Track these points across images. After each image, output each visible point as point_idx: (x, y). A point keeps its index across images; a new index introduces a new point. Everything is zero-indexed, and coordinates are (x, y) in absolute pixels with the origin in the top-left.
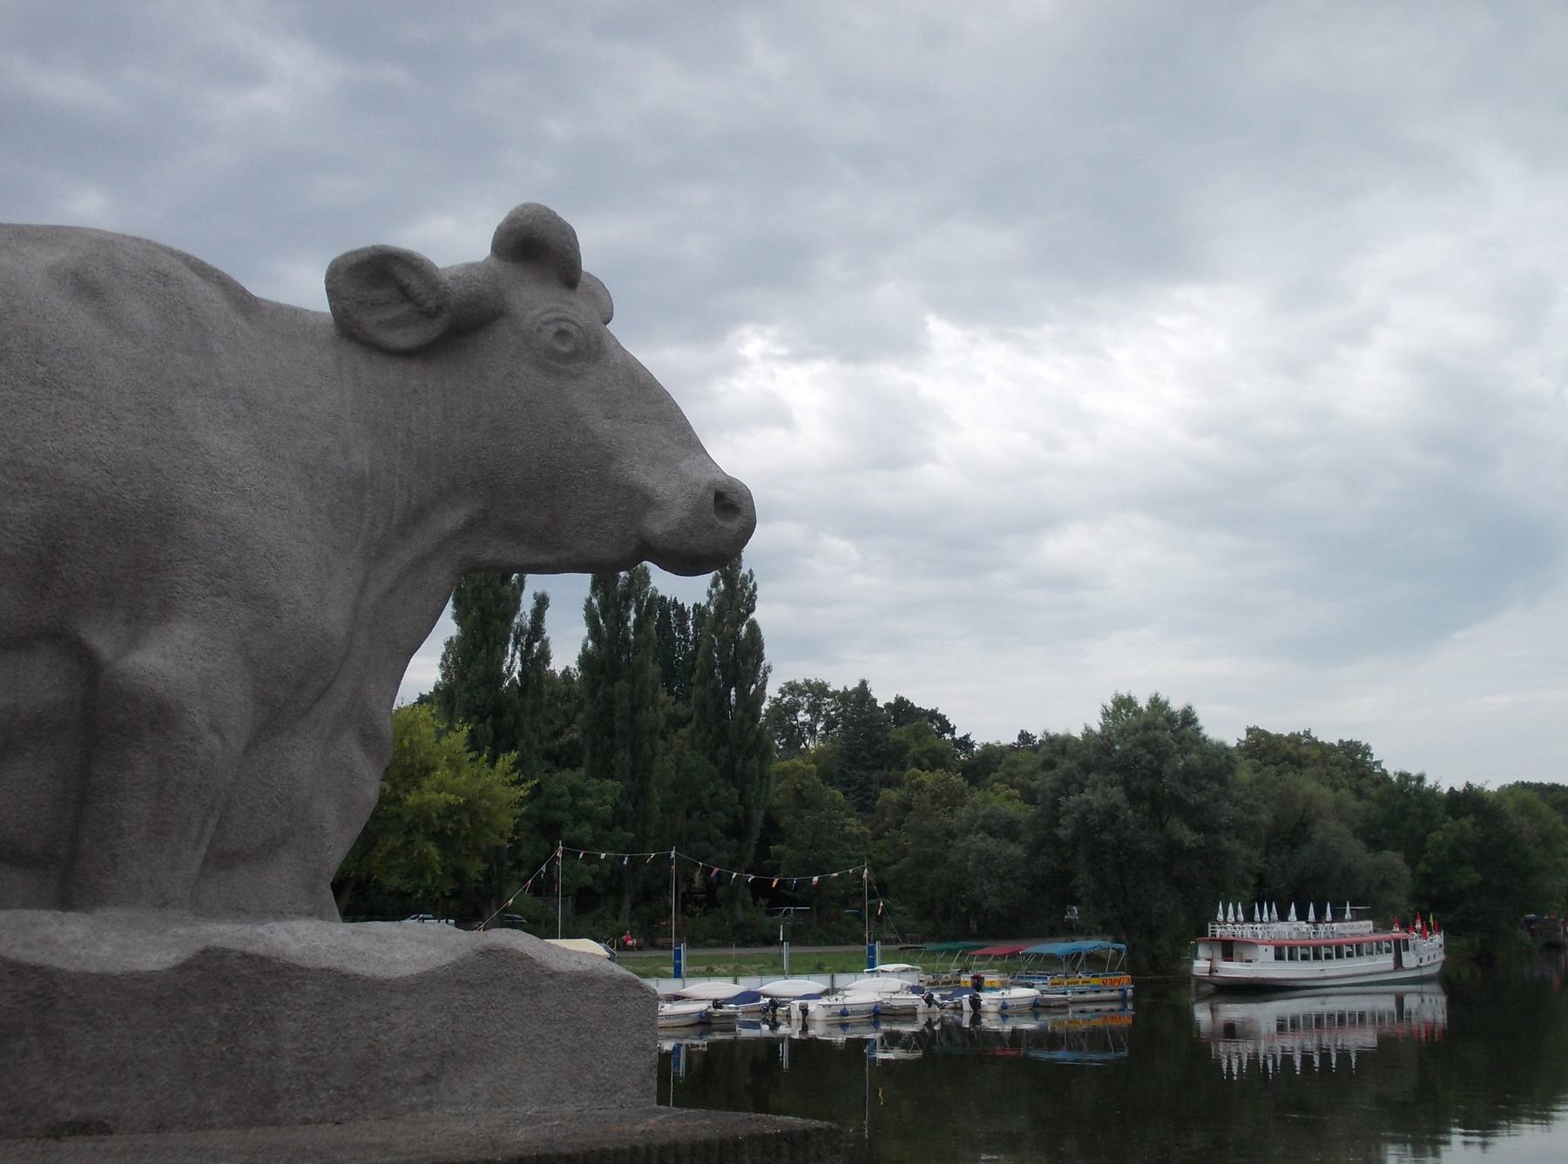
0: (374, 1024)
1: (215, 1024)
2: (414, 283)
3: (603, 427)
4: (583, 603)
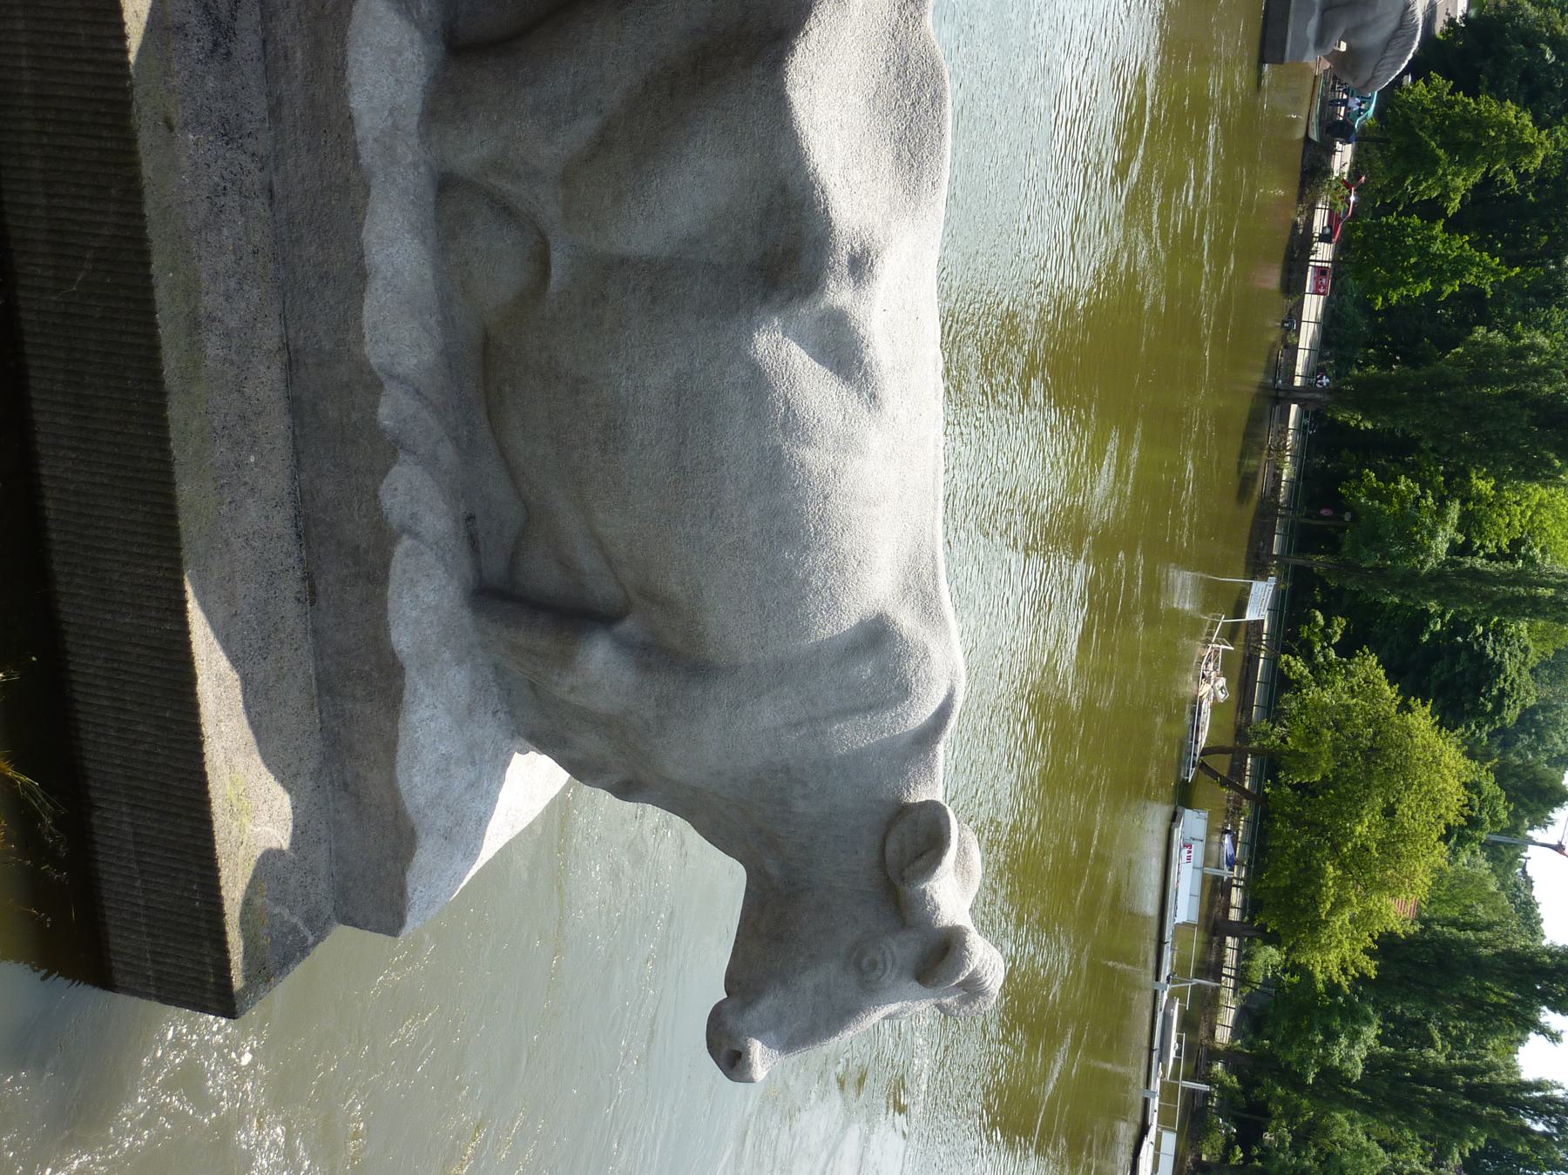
0: (372, 758)
1: (367, 668)
2: (921, 863)
3: (808, 981)
4: (1559, 1079)
